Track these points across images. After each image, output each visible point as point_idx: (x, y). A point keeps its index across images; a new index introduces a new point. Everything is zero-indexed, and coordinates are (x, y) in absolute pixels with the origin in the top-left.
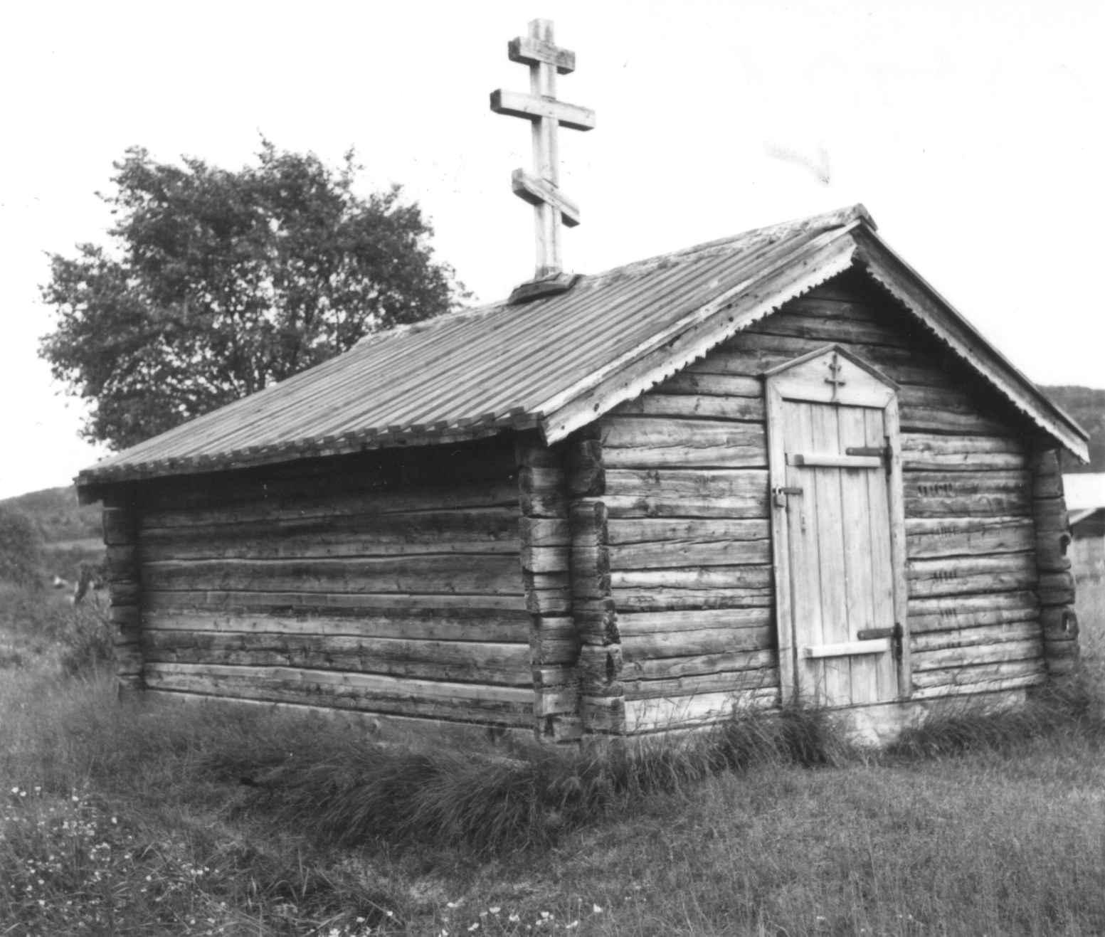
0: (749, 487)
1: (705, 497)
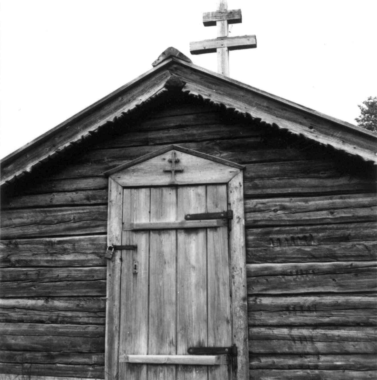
0: (90, 246)
1: (52, 254)
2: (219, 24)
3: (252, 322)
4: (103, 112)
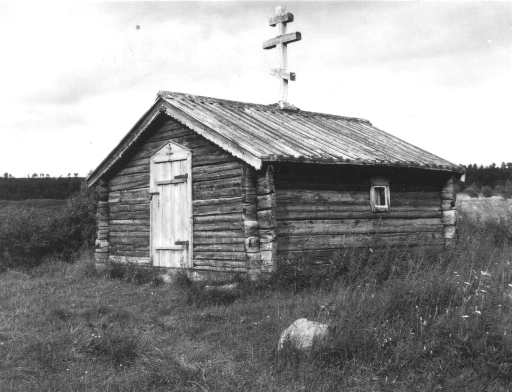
2: (277, 25)
3: (195, 229)
4: (142, 125)
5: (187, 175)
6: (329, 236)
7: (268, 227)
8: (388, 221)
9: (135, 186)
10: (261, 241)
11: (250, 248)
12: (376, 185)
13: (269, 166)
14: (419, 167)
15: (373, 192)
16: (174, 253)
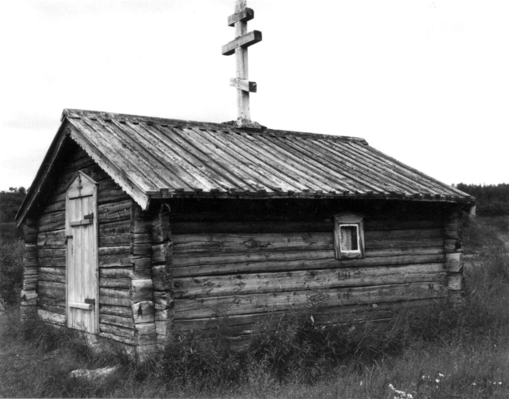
2: (236, 25)
5: (93, 214)
6: (268, 294)
7: (163, 289)
8: (364, 271)
9: (56, 227)
10: (156, 308)
11: (140, 317)
12: (342, 223)
13: (162, 205)
14: (404, 198)
15: (338, 234)
16: (85, 313)
